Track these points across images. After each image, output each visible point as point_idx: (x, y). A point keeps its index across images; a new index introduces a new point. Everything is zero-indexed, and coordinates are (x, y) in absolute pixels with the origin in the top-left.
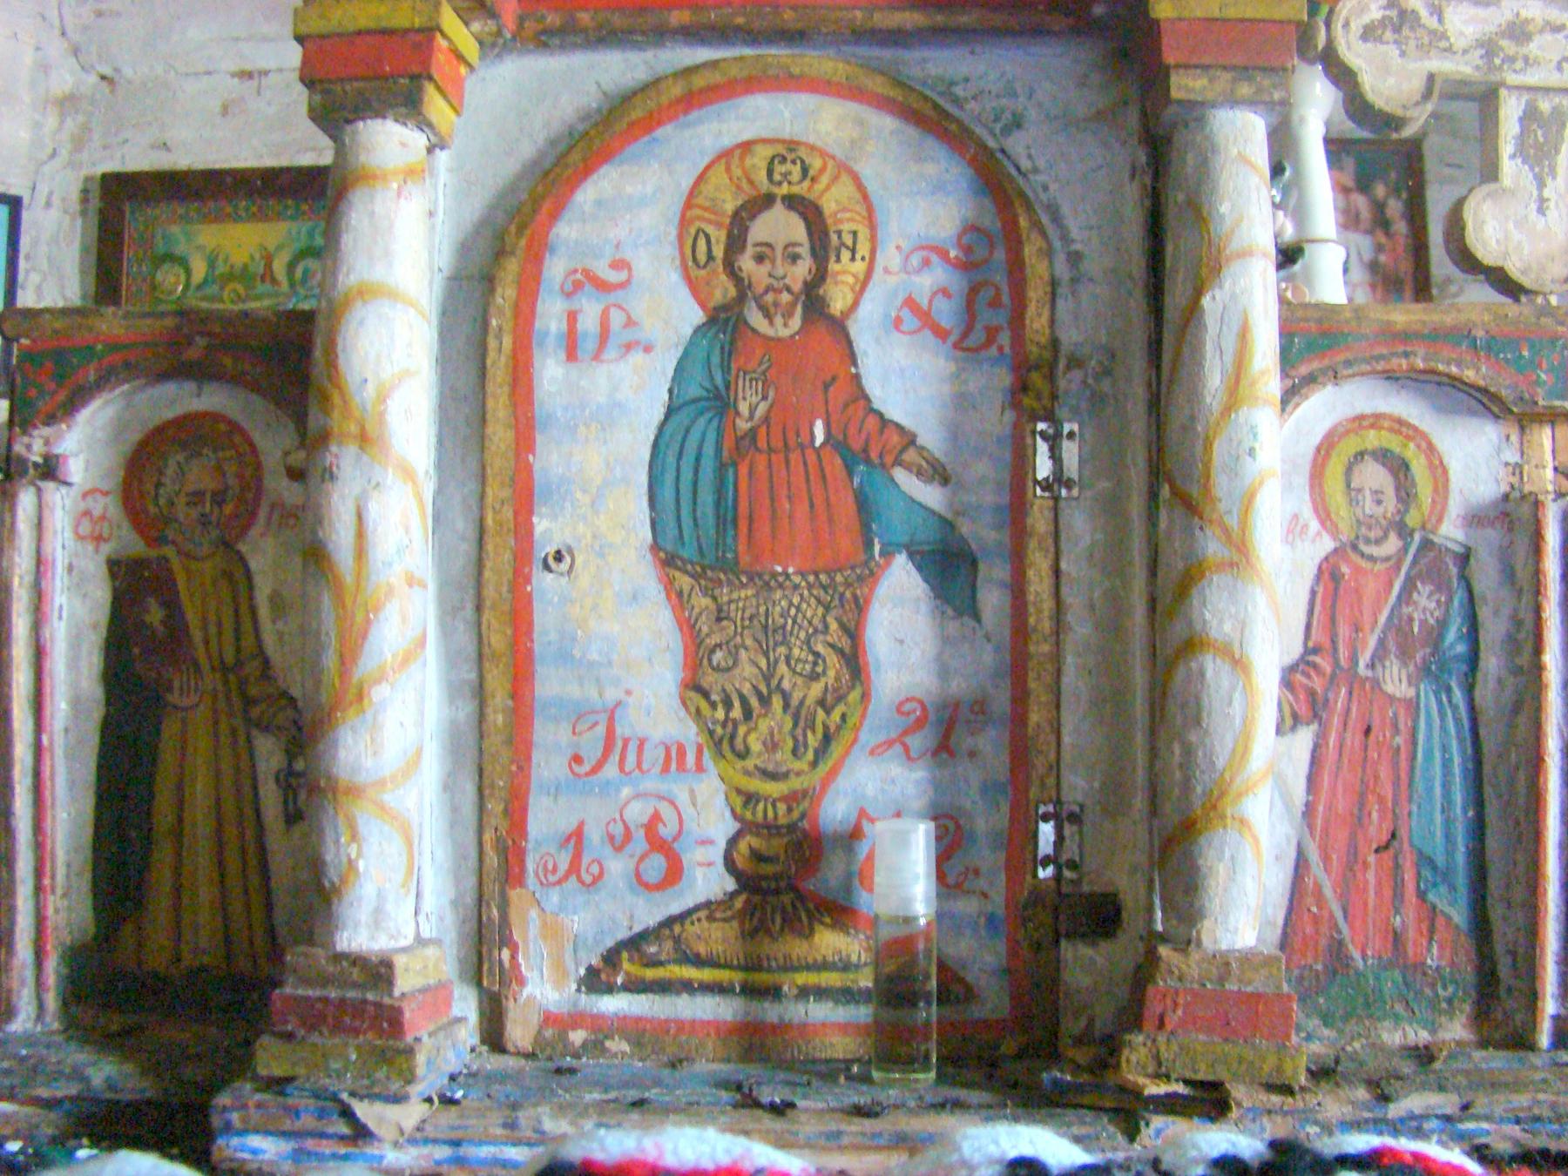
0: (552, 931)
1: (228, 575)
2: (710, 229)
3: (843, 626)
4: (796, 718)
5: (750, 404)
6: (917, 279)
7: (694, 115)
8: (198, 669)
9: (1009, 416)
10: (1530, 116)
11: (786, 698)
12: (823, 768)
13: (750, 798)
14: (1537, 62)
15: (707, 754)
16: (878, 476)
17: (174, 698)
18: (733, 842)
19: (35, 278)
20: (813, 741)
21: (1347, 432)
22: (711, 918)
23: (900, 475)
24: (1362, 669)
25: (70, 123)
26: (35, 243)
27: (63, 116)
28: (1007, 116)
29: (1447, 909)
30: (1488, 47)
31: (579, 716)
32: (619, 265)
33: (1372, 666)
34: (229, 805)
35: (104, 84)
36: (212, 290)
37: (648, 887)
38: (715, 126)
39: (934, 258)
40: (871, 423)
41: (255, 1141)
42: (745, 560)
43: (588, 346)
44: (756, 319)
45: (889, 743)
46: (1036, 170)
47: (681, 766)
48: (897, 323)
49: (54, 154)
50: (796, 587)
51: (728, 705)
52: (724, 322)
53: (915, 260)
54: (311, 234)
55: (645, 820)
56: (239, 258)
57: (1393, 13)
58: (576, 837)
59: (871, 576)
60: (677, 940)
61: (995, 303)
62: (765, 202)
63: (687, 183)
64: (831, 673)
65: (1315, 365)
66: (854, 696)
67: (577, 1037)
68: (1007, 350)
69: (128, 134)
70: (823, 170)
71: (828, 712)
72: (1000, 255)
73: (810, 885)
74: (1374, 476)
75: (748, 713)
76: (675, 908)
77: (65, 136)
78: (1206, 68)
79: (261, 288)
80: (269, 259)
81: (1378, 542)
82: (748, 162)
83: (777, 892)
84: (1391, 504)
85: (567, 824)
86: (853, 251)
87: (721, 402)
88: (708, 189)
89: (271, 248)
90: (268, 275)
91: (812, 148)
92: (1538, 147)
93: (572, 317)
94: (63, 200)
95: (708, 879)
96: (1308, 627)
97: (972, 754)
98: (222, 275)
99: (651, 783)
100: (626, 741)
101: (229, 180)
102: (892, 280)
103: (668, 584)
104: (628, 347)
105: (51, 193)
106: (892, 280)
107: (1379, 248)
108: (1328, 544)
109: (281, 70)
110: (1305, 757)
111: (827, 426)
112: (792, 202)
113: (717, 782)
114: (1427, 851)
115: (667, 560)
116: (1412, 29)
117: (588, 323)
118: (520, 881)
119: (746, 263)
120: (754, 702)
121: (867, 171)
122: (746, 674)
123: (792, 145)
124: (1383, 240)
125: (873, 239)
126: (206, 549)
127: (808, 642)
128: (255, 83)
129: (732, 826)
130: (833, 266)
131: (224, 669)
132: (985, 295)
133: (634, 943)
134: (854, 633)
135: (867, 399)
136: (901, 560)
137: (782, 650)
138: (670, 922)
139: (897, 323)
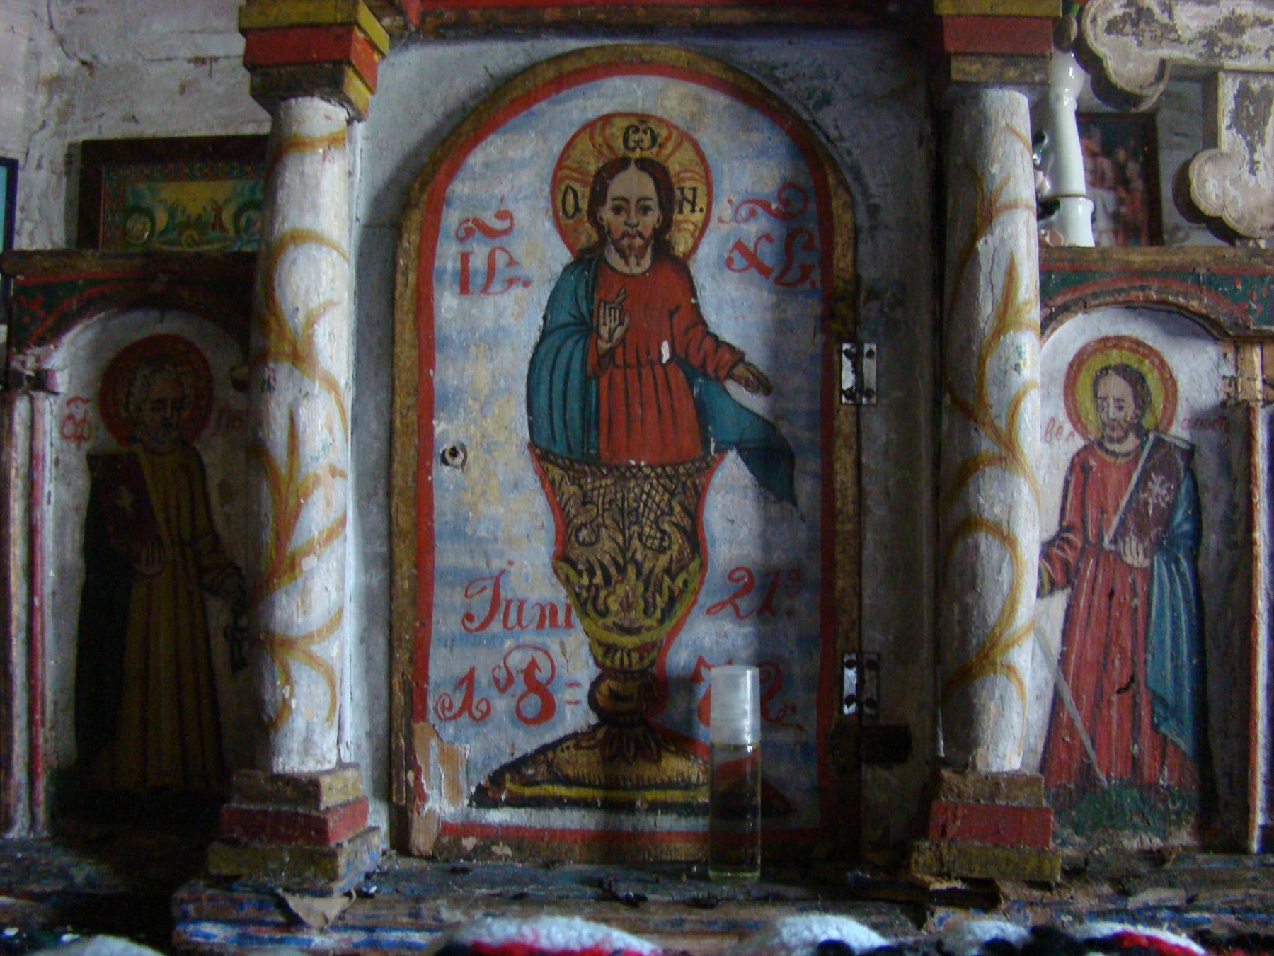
0: (448, 756)
5: (609, 328)
7: (564, 93)
13: (609, 649)
25: (56, 100)
27: (51, 95)
31: (471, 582)
35: (85, 68)
36: (172, 236)
38: (581, 102)
43: (478, 281)
44: (614, 259)
46: (842, 138)
48: (729, 263)
49: (44, 126)
52: (588, 264)
54: (252, 191)
56: (194, 209)
58: (468, 681)
59: (707, 468)
61: (808, 247)
62: (620, 164)
67: (469, 843)
69: (103, 109)
72: (812, 207)
76: (549, 738)
77: (53, 110)
79: (212, 234)
80: (218, 211)
84: (1130, 409)
85: (460, 670)
87: (586, 327)
89: (220, 202)
90: (218, 224)
93: (465, 258)
94: (52, 162)
95: (574, 715)
99: (529, 637)
101: (186, 146)
104: (511, 282)
105: (41, 157)
107: (1120, 202)
108: (1079, 443)
109: (228, 57)
112: (644, 164)
115: (541, 453)
117: (478, 262)
118: (423, 716)
119: (607, 214)
121: (704, 139)
123: (644, 118)
124: (1124, 195)
133: (515, 767)
134: (694, 514)
136: (732, 455)
138: (544, 749)
139: (729, 263)
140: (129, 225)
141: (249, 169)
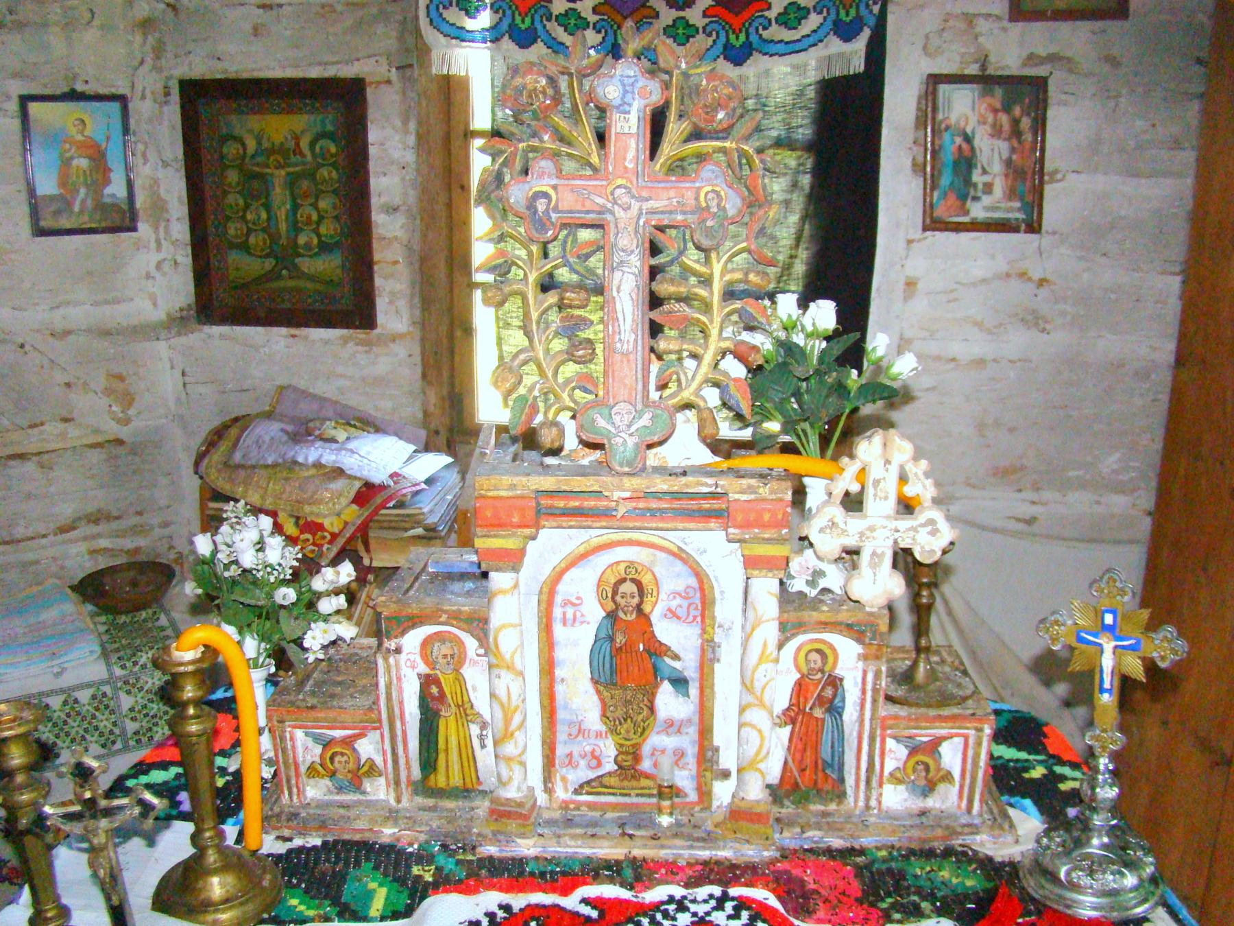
0: (564, 779)
5: (620, 639)
9: (700, 641)
10: (874, 554)
13: (621, 745)
17: (442, 713)
25: (151, 39)
26: (138, 122)
27: (145, 35)
30: (862, 534)
31: (570, 724)
32: (578, 598)
35: (170, 10)
36: (260, 159)
43: (569, 622)
44: (621, 614)
48: (665, 616)
49: (142, 62)
52: (612, 616)
54: (323, 122)
56: (278, 139)
58: (570, 755)
59: (657, 686)
61: (696, 609)
62: (623, 580)
67: (572, 806)
69: (190, 47)
72: (698, 595)
73: (639, 767)
74: (815, 656)
76: (600, 773)
77: (148, 48)
79: (293, 159)
80: (297, 139)
84: (819, 663)
85: (567, 751)
87: (611, 639)
89: (298, 132)
90: (297, 151)
93: (564, 614)
94: (152, 93)
95: (609, 766)
98: (266, 149)
99: (592, 741)
101: (265, 87)
104: (582, 622)
105: (144, 88)
107: (1013, 150)
108: (798, 676)
109: (290, 4)
110: (788, 734)
112: (633, 580)
115: (595, 682)
117: (570, 615)
118: (554, 766)
119: (618, 598)
121: (656, 570)
122: (620, 713)
123: (632, 562)
124: (1016, 145)
128: (274, 13)
129: (616, 753)
131: (458, 706)
132: (692, 608)
133: (589, 782)
134: (652, 701)
136: (666, 682)
138: (599, 777)
139: (665, 616)
140: (225, 150)
141: (318, 105)
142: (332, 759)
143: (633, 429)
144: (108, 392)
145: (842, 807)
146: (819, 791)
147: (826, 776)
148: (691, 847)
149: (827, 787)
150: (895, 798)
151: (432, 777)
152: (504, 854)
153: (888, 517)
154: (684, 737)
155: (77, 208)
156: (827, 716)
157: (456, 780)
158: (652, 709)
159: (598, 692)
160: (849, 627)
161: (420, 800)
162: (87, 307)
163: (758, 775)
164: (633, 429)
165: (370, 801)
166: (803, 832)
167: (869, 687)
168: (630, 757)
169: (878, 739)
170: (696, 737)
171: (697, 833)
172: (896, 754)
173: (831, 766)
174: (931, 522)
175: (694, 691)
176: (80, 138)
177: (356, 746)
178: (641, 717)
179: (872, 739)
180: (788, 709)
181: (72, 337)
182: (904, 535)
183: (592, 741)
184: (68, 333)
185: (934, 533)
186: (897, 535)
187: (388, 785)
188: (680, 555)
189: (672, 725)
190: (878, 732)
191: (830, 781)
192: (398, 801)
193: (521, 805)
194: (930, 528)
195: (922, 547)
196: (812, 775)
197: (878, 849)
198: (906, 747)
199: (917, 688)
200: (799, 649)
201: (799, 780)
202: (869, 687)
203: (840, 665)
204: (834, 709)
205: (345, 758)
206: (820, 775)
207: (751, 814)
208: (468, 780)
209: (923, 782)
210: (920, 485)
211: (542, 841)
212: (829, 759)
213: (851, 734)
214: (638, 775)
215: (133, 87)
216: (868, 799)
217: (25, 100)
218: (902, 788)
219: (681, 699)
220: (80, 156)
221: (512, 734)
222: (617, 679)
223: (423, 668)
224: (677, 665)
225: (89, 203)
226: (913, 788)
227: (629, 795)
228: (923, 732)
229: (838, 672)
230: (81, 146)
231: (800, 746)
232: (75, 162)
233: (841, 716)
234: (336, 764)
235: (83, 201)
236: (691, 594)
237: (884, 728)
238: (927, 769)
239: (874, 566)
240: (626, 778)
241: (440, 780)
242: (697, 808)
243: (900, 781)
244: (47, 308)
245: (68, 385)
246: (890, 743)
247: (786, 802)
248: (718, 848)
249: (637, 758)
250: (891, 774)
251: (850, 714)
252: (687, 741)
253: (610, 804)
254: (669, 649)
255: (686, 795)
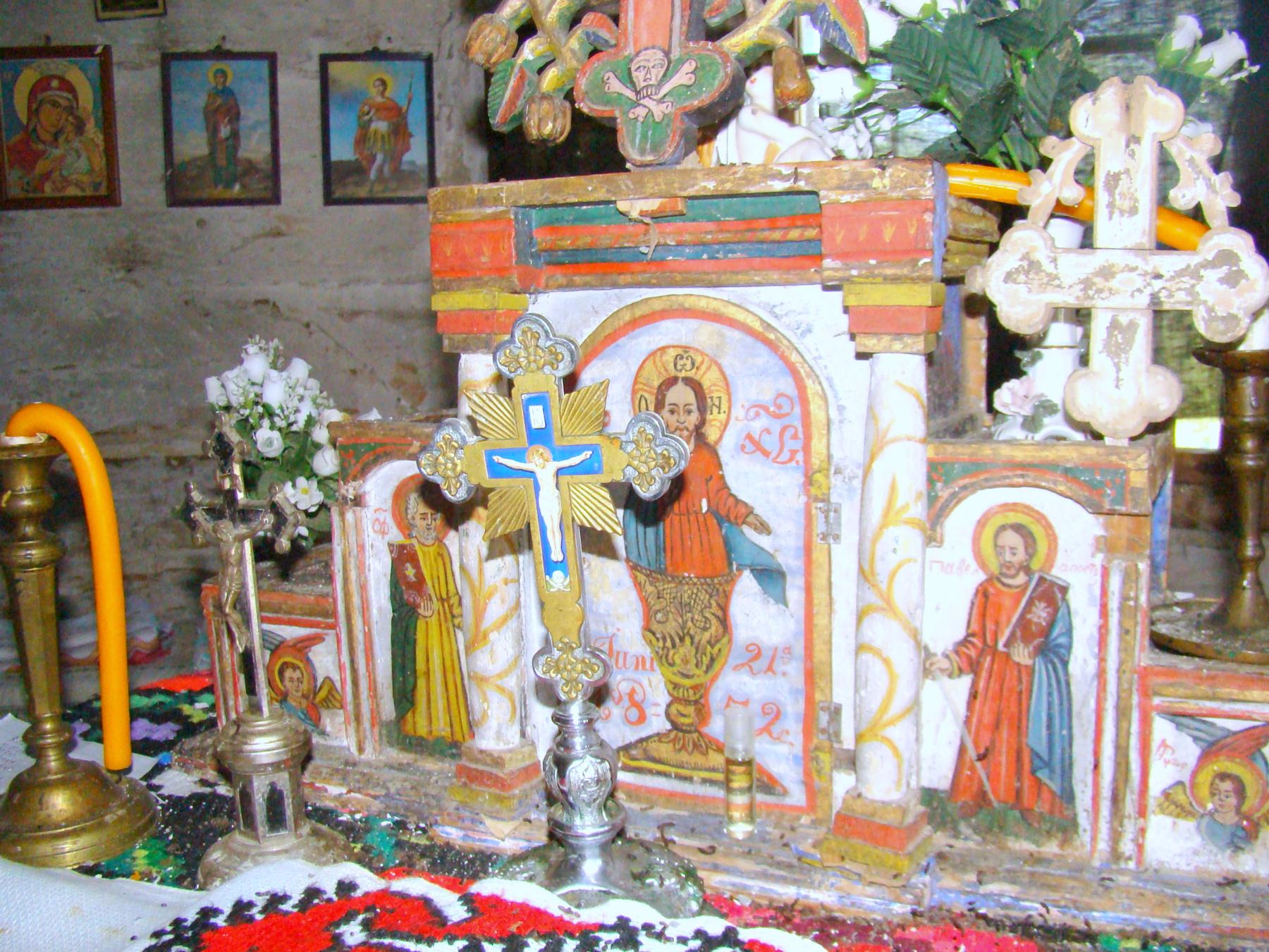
1: (441, 555)
2: (646, 395)
3: (719, 605)
4: (697, 649)
6: (752, 423)
8: (431, 599)
9: (803, 499)
10: (1114, 325)
11: (692, 638)
12: (710, 674)
13: (676, 686)
14: (1118, 292)
15: (655, 664)
16: (734, 528)
18: (669, 706)
19: (446, 111)
20: (706, 660)
21: (996, 513)
22: (660, 741)
23: (745, 529)
24: (1000, 646)
26: (444, 85)
28: (803, 327)
29: (1048, 782)
30: (1087, 284)
33: (1007, 645)
34: (448, 664)
37: (632, 723)
39: (762, 412)
40: (731, 501)
41: (448, 829)
42: (670, 569)
45: (743, 665)
46: (820, 358)
47: (644, 665)
48: (743, 448)
50: (695, 584)
51: (664, 639)
53: (752, 413)
55: (628, 691)
57: (1025, 263)
59: (732, 581)
60: (645, 750)
61: (795, 437)
62: (672, 381)
63: (634, 369)
64: (713, 628)
65: (967, 481)
66: (725, 640)
68: (801, 463)
70: (702, 363)
71: (712, 647)
72: (797, 410)
73: (705, 730)
74: (1011, 538)
75: (674, 646)
76: (644, 734)
78: (876, 334)
81: (1013, 577)
82: (665, 358)
83: (690, 732)
84: (1021, 556)
86: (719, 408)
88: (645, 373)
91: (697, 350)
92: (1118, 345)
95: (658, 723)
96: (969, 622)
97: (784, 674)
100: (618, 653)
102: (740, 424)
103: (635, 578)
105: (451, 47)
106: (740, 424)
108: (981, 577)
111: (709, 502)
112: (689, 381)
113: (660, 677)
114: (1037, 749)
116: (1037, 273)
120: (677, 640)
121: (725, 362)
122: (672, 627)
123: (686, 349)
125: (730, 400)
126: (430, 542)
127: (702, 611)
129: (668, 699)
130: (709, 417)
131: (442, 600)
132: (788, 434)
134: (724, 608)
135: (729, 489)
137: (689, 615)
138: (641, 740)
142: (281, 673)
143: (666, 89)
144: (398, 383)
145: (1068, 850)
146: (1026, 814)
147: (1039, 784)
148: (764, 876)
149: (1040, 807)
150: (1173, 844)
151: (409, 715)
152: (469, 844)
153: (1137, 250)
154: (780, 680)
155: (373, 174)
156: (1040, 665)
157: (441, 727)
158: (724, 621)
159: (638, 585)
160: (1069, 474)
161: (395, 754)
162: (378, 286)
163: (886, 751)
164: (666, 89)
165: (331, 747)
166: (980, 882)
167: (1114, 604)
168: (691, 710)
169: (1135, 715)
170: (799, 681)
171: (783, 856)
172: (1172, 755)
173: (1048, 764)
174: (1226, 257)
175: (795, 594)
176: (379, 99)
177: (311, 655)
178: (707, 635)
179: (1122, 713)
180: (965, 642)
181: (362, 319)
182: (1172, 285)
183: (630, 674)
184: (355, 314)
185: (1234, 279)
186: (1157, 284)
187: (347, 721)
188: (766, 338)
189: (758, 655)
190: (1135, 699)
191: (1045, 795)
192: (361, 749)
193: (498, 761)
194: (1225, 269)
195: (1210, 310)
196: (1012, 783)
197: (1125, 935)
198: (1196, 739)
199: (1235, 632)
200: (982, 524)
201: (987, 786)
202: (1114, 604)
203: (1060, 559)
204: (1050, 645)
205: (297, 674)
206: (1027, 782)
207: (869, 824)
208: (457, 728)
209: (1231, 818)
210: (1201, 184)
211: (526, 828)
212: (1042, 750)
213: (1085, 703)
214: (706, 745)
215: (439, 45)
216: (1115, 837)
217: (325, 60)
218: (1188, 825)
219: (773, 608)
220: (379, 119)
221: (485, 636)
222: (666, 561)
223: (396, 536)
224: (764, 541)
225: (386, 169)
226: (1211, 827)
227: (688, 779)
228: (1227, 707)
229: (1058, 573)
230: (380, 108)
231: (988, 719)
232: (374, 126)
233: (1065, 663)
234: (288, 683)
235: (380, 171)
236: (786, 409)
237: (1145, 693)
238: (1240, 791)
239: (1117, 351)
240: (683, 747)
241: (419, 724)
242: (805, 820)
243: (1183, 812)
244: (336, 284)
245: (354, 372)
246: (1162, 728)
247: (963, 828)
248: (811, 885)
249: (703, 712)
250: (1166, 794)
251: (1081, 661)
252: (784, 688)
253: (660, 792)
254: (750, 511)
255: (785, 792)
